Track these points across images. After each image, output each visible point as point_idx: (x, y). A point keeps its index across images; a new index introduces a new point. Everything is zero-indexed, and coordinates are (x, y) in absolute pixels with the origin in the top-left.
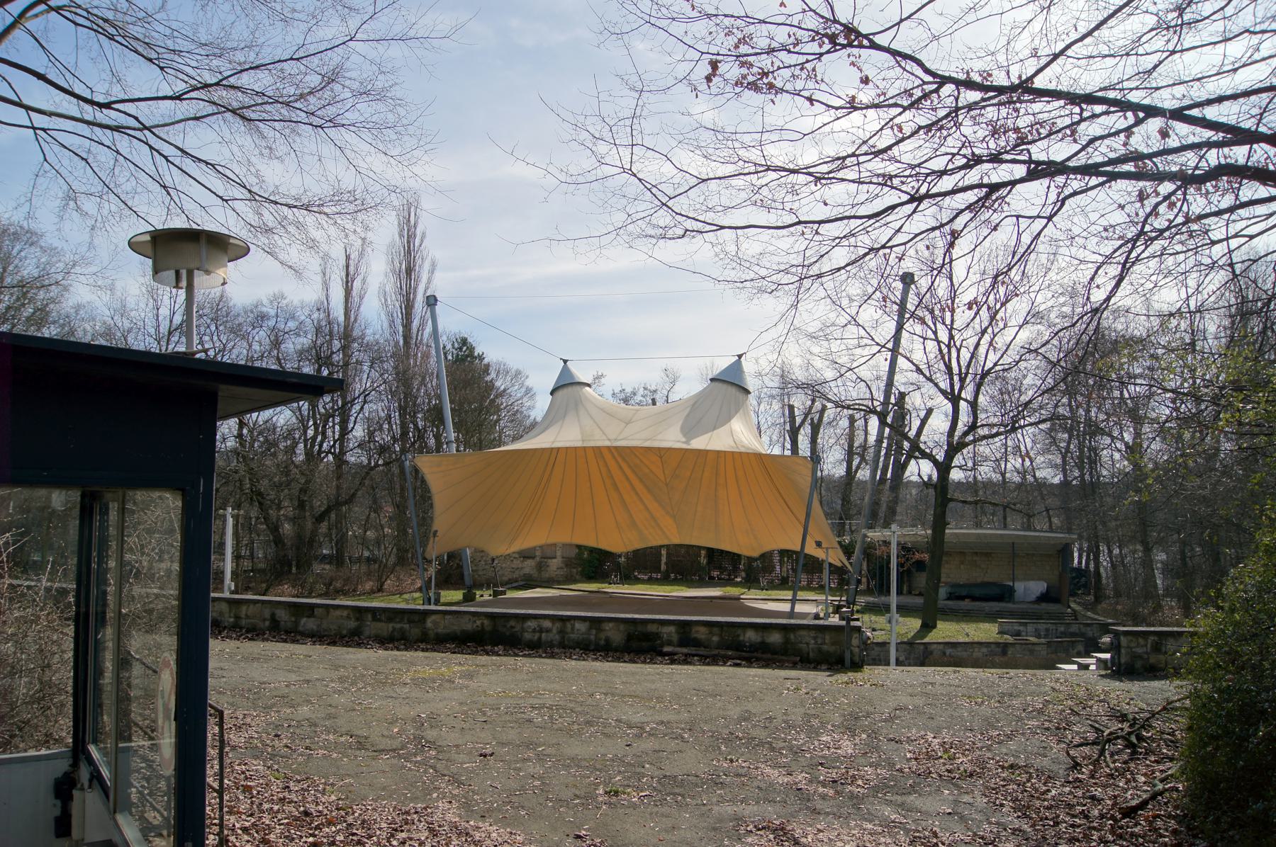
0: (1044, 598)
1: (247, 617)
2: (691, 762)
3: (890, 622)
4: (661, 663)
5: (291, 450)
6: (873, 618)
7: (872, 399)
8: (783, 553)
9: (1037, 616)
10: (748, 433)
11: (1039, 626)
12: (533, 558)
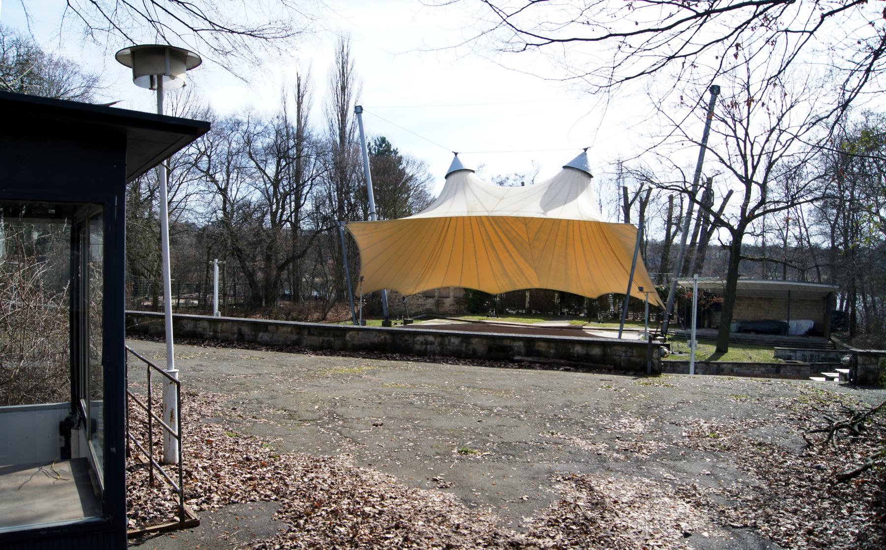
0: (811, 332)
1: (222, 331)
2: (523, 433)
3: (690, 346)
4: (512, 367)
5: (261, 220)
6: (681, 344)
7: (685, 182)
8: (617, 296)
9: (805, 346)
10: (594, 205)
11: (806, 353)
12: (433, 297)
